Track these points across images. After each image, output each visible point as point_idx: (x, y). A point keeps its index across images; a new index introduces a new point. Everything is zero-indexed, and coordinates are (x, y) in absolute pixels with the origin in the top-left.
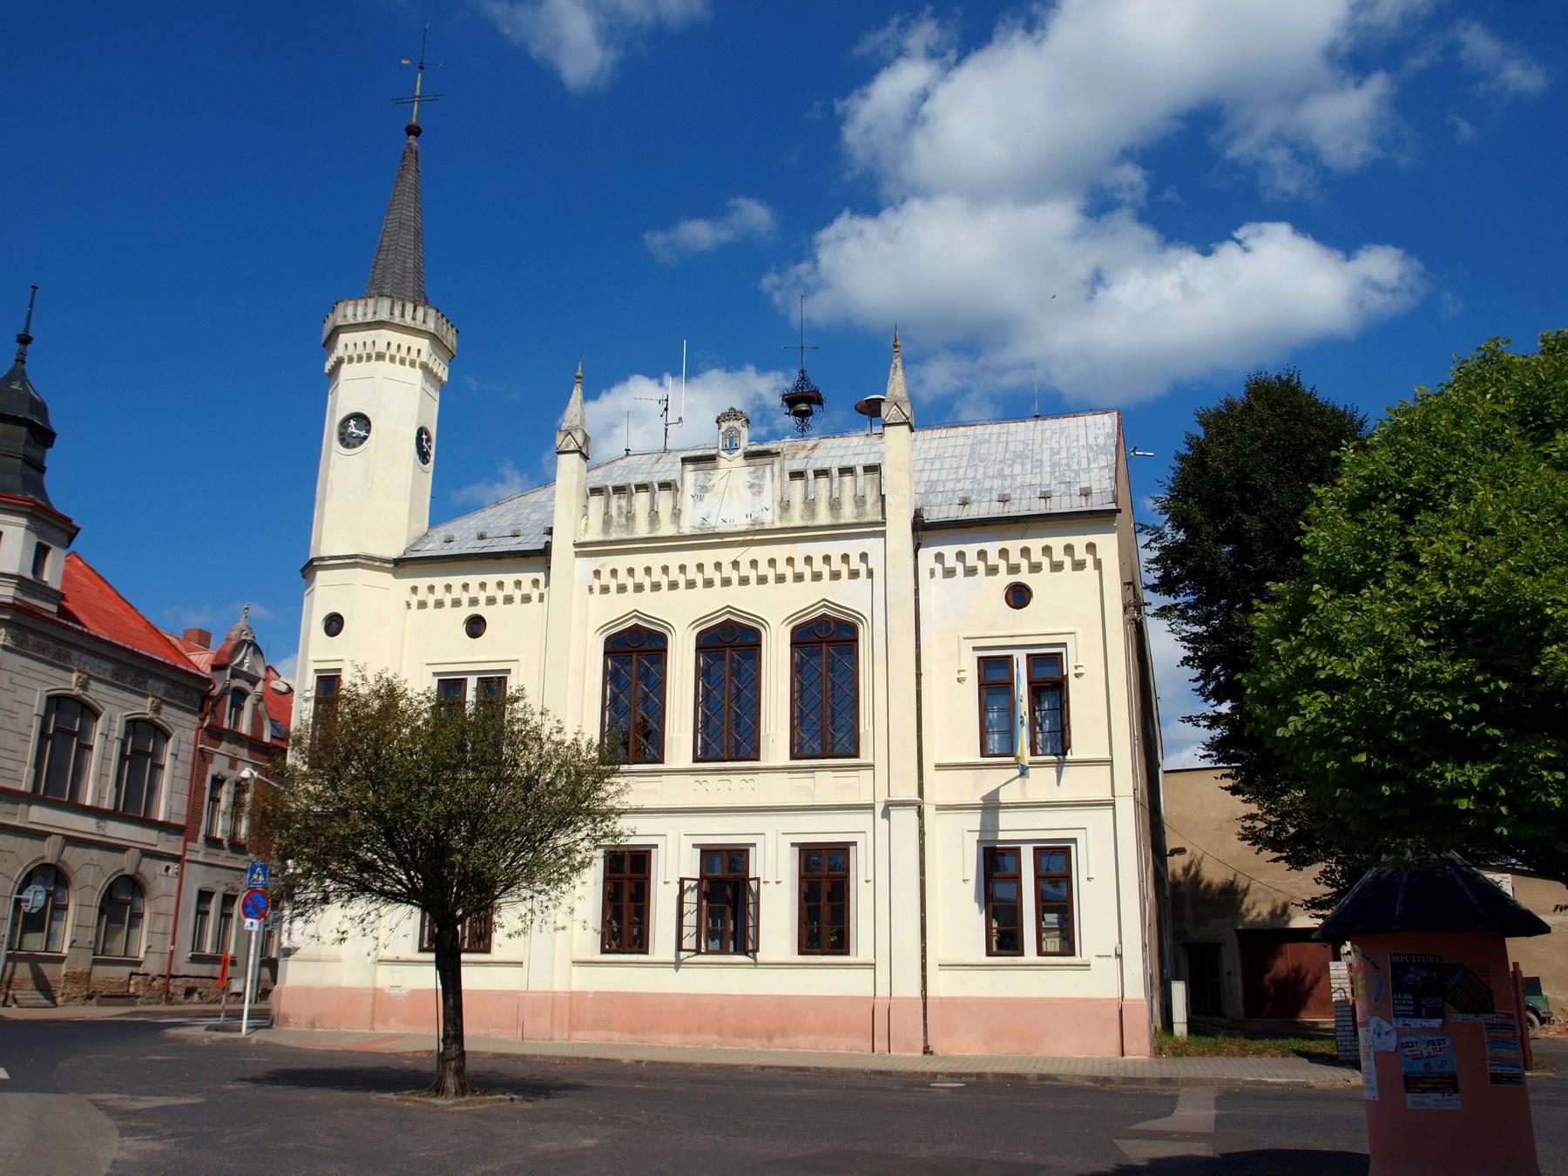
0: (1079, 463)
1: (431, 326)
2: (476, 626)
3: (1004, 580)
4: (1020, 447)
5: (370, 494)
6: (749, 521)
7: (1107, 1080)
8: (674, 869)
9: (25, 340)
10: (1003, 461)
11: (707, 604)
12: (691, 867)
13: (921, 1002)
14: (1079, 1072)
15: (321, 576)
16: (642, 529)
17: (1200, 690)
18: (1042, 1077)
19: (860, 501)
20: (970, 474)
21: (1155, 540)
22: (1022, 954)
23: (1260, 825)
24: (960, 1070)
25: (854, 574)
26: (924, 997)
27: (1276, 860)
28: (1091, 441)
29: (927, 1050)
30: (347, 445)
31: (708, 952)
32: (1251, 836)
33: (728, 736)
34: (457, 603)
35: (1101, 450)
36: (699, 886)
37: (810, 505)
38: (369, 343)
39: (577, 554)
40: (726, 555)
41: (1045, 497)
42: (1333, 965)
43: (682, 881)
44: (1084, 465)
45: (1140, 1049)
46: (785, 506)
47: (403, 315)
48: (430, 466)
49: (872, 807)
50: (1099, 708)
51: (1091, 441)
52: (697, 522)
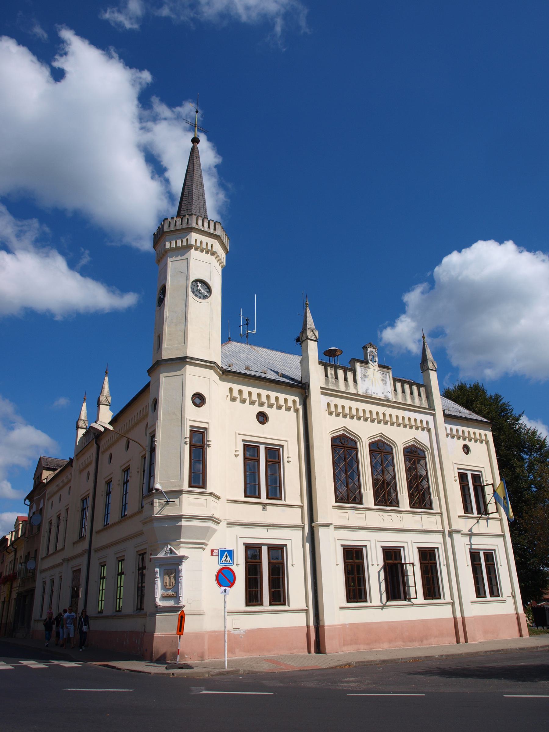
3: (257, 409)
39: (322, 393)
50: (225, 468)
52: (364, 391)
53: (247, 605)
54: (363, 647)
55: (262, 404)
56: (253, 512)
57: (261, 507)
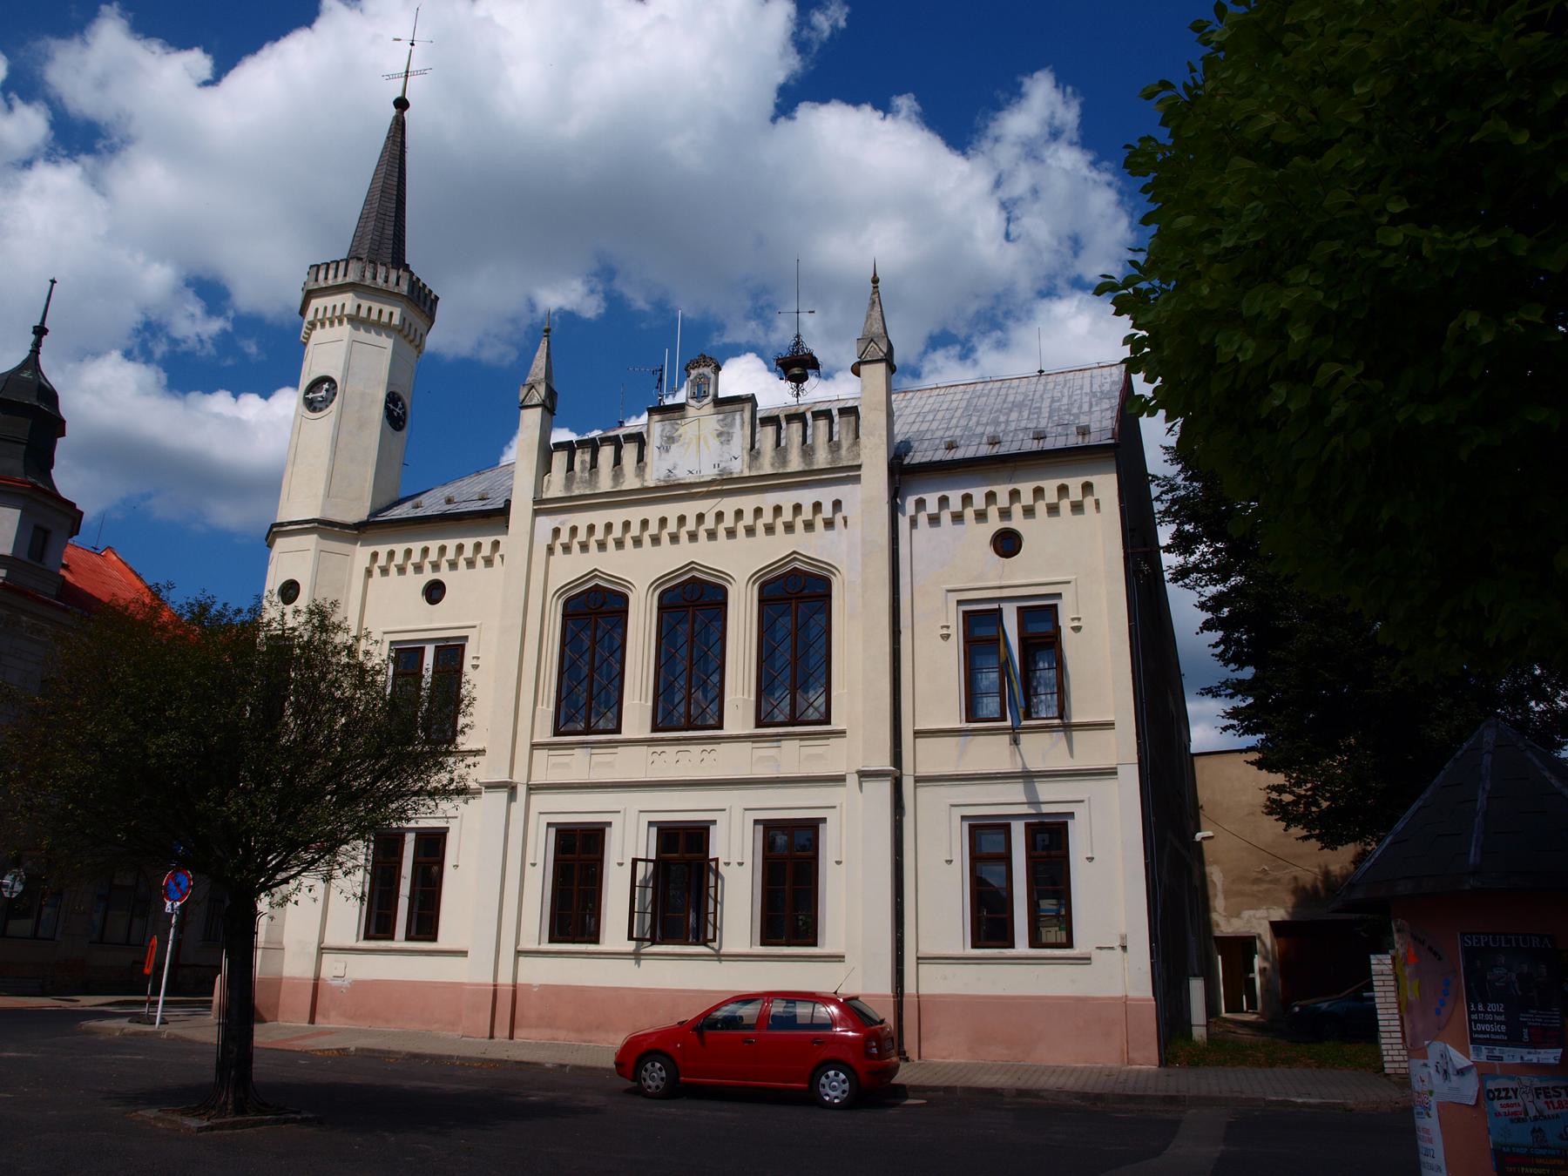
0: (1080, 407)
2: (434, 592)
4: (1020, 398)
6: (716, 471)
8: (628, 848)
9: (40, 331)
11: (669, 559)
17: (1221, 656)
18: (1021, 1093)
20: (963, 422)
21: (1166, 493)
22: (1012, 946)
23: (1287, 798)
24: (927, 1083)
27: (1305, 838)
28: (1096, 388)
30: (314, 410)
32: (1275, 808)
33: (687, 704)
35: (1106, 395)
40: (690, 509)
43: (635, 861)
44: (1086, 407)
45: (1146, 1059)
51: (1096, 388)
52: (662, 474)
54: (563, 1036)
56: (991, 753)
57: (1006, 739)
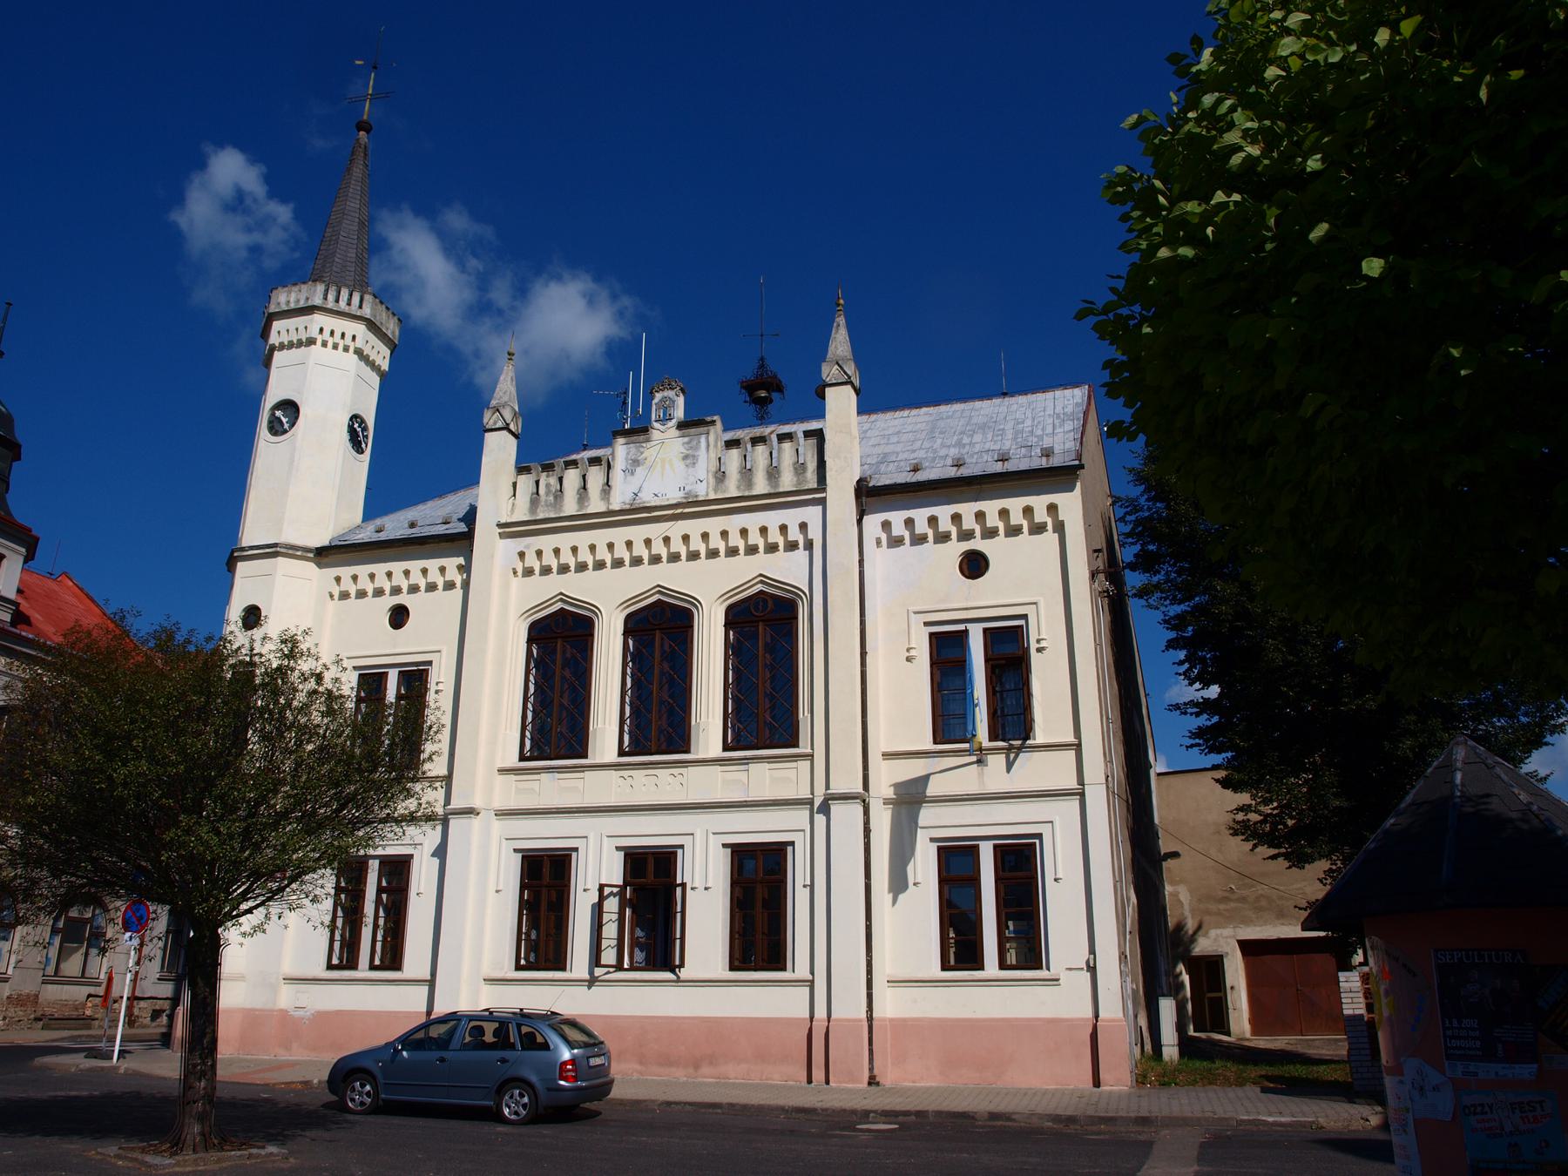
1: (367, 311)
3: (956, 548)
5: (305, 482)
6: (682, 494)
7: (1071, 1120)
8: (598, 869)
10: (963, 433)
11: (638, 584)
12: (614, 873)
13: (865, 1024)
14: (1039, 1111)
15: (241, 567)
16: (570, 507)
18: (994, 1116)
19: (800, 468)
23: (1254, 817)
25: (792, 546)
26: (870, 1019)
27: (1273, 857)
29: (872, 1081)
31: (632, 968)
32: (1241, 829)
34: (379, 592)
36: (622, 894)
37: (747, 473)
38: (301, 328)
40: (655, 531)
41: (1003, 459)
42: (1342, 976)
43: (601, 887)
44: (1049, 429)
45: (1118, 1078)
46: (720, 476)
47: (337, 301)
48: (366, 456)
49: (810, 802)
50: (1068, 685)
52: (628, 497)
53: (732, 968)
55: (966, 535)
